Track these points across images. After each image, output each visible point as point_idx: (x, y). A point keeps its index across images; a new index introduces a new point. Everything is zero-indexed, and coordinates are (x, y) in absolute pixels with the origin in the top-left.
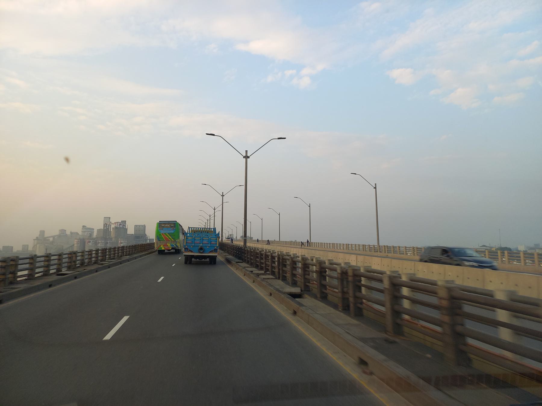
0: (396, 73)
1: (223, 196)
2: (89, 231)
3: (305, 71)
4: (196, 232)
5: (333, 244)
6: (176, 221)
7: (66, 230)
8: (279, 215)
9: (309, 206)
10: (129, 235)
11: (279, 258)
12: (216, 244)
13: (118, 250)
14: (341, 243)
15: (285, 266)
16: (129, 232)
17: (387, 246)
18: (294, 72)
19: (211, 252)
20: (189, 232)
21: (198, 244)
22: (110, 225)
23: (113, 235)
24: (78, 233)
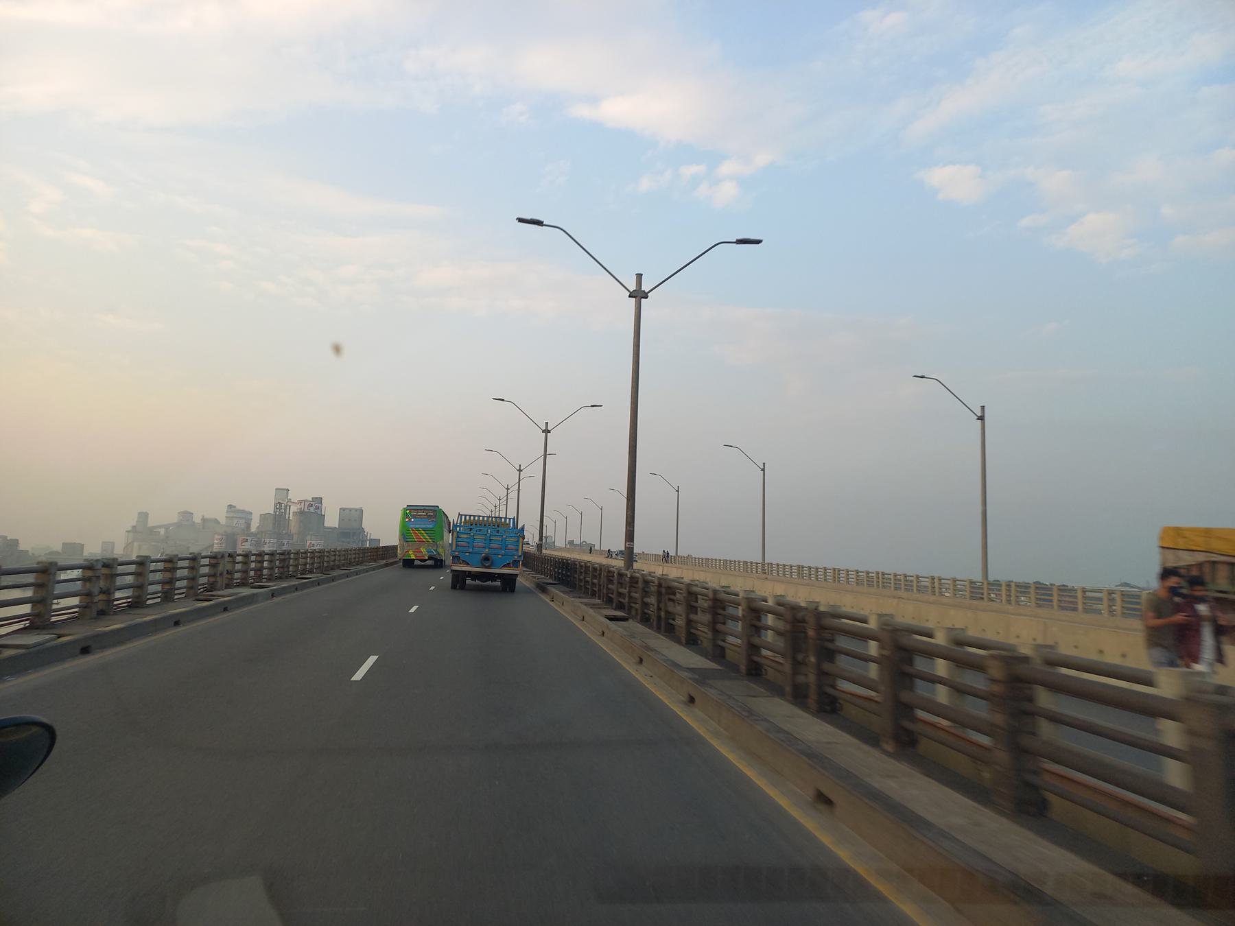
0: (938, 176)
2: (240, 518)
3: (727, 168)
4: (475, 525)
6: (438, 507)
7: (192, 514)
8: (763, 470)
9: (762, 470)
12: (518, 550)
14: (787, 564)
16: (327, 524)
17: (883, 574)
21: (480, 550)
22: (288, 507)
23: (294, 527)
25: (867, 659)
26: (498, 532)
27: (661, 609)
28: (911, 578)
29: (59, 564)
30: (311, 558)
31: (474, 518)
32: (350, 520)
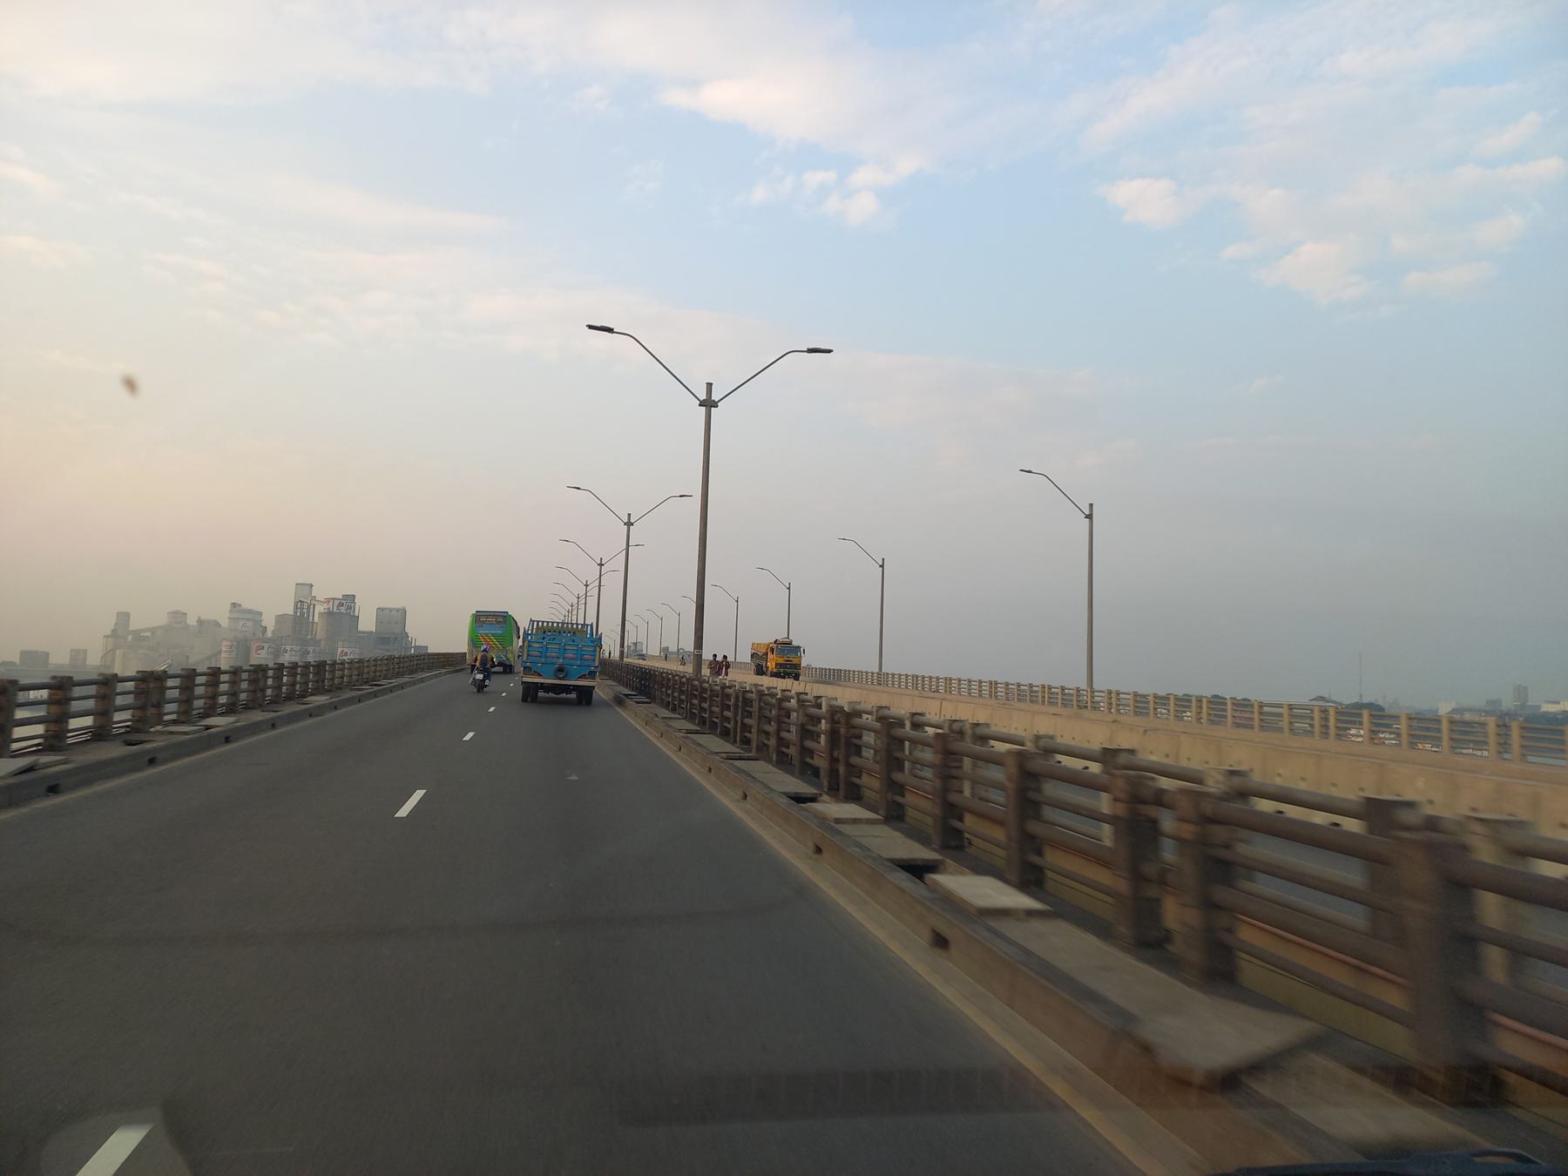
0: (1126, 192)
1: (629, 524)
2: (248, 620)
3: (861, 177)
4: (547, 632)
5: (948, 680)
8: (737, 601)
9: (880, 566)
10: (363, 632)
11: (833, 721)
12: (594, 660)
13: (305, 675)
15: (858, 750)
17: (1050, 688)
18: (829, 176)
19: (583, 677)
20: (532, 630)
22: (311, 606)
23: (320, 633)
24: (220, 623)
25: (1098, 817)
26: (574, 641)
27: (838, 760)
28: (1056, 690)
29: (75, 679)
30: (350, 669)
31: (543, 624)
32: (390, 623)
